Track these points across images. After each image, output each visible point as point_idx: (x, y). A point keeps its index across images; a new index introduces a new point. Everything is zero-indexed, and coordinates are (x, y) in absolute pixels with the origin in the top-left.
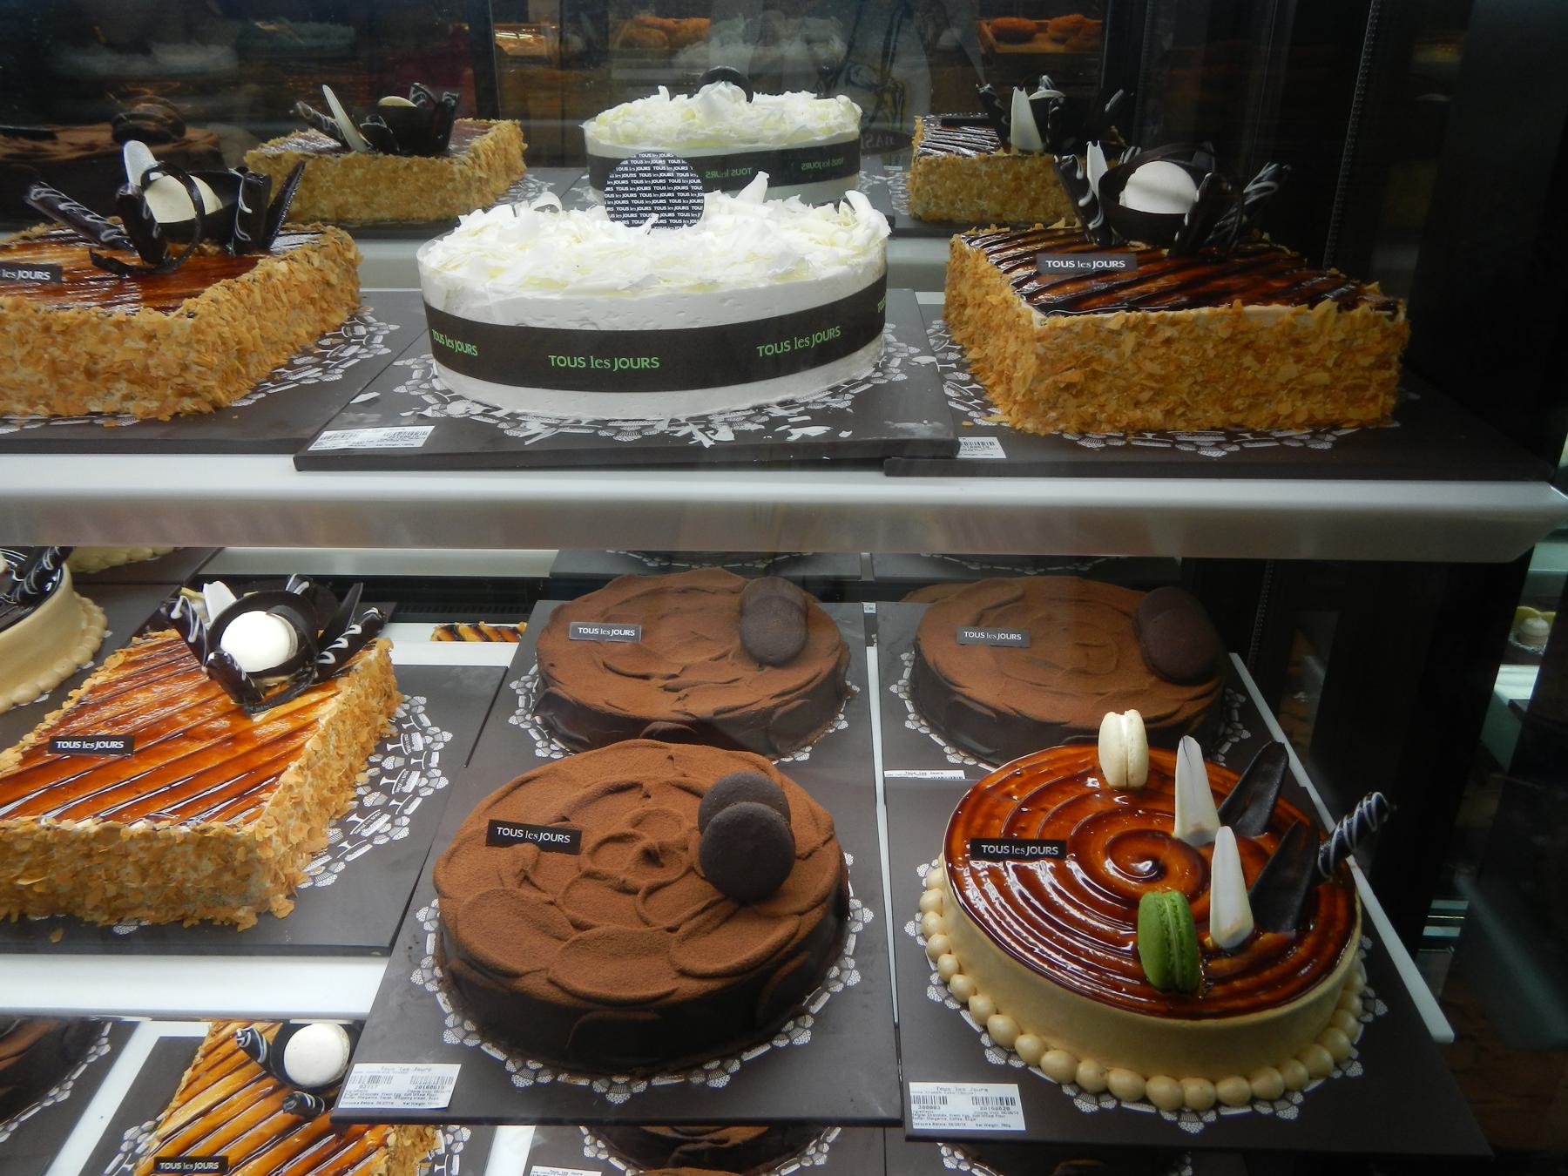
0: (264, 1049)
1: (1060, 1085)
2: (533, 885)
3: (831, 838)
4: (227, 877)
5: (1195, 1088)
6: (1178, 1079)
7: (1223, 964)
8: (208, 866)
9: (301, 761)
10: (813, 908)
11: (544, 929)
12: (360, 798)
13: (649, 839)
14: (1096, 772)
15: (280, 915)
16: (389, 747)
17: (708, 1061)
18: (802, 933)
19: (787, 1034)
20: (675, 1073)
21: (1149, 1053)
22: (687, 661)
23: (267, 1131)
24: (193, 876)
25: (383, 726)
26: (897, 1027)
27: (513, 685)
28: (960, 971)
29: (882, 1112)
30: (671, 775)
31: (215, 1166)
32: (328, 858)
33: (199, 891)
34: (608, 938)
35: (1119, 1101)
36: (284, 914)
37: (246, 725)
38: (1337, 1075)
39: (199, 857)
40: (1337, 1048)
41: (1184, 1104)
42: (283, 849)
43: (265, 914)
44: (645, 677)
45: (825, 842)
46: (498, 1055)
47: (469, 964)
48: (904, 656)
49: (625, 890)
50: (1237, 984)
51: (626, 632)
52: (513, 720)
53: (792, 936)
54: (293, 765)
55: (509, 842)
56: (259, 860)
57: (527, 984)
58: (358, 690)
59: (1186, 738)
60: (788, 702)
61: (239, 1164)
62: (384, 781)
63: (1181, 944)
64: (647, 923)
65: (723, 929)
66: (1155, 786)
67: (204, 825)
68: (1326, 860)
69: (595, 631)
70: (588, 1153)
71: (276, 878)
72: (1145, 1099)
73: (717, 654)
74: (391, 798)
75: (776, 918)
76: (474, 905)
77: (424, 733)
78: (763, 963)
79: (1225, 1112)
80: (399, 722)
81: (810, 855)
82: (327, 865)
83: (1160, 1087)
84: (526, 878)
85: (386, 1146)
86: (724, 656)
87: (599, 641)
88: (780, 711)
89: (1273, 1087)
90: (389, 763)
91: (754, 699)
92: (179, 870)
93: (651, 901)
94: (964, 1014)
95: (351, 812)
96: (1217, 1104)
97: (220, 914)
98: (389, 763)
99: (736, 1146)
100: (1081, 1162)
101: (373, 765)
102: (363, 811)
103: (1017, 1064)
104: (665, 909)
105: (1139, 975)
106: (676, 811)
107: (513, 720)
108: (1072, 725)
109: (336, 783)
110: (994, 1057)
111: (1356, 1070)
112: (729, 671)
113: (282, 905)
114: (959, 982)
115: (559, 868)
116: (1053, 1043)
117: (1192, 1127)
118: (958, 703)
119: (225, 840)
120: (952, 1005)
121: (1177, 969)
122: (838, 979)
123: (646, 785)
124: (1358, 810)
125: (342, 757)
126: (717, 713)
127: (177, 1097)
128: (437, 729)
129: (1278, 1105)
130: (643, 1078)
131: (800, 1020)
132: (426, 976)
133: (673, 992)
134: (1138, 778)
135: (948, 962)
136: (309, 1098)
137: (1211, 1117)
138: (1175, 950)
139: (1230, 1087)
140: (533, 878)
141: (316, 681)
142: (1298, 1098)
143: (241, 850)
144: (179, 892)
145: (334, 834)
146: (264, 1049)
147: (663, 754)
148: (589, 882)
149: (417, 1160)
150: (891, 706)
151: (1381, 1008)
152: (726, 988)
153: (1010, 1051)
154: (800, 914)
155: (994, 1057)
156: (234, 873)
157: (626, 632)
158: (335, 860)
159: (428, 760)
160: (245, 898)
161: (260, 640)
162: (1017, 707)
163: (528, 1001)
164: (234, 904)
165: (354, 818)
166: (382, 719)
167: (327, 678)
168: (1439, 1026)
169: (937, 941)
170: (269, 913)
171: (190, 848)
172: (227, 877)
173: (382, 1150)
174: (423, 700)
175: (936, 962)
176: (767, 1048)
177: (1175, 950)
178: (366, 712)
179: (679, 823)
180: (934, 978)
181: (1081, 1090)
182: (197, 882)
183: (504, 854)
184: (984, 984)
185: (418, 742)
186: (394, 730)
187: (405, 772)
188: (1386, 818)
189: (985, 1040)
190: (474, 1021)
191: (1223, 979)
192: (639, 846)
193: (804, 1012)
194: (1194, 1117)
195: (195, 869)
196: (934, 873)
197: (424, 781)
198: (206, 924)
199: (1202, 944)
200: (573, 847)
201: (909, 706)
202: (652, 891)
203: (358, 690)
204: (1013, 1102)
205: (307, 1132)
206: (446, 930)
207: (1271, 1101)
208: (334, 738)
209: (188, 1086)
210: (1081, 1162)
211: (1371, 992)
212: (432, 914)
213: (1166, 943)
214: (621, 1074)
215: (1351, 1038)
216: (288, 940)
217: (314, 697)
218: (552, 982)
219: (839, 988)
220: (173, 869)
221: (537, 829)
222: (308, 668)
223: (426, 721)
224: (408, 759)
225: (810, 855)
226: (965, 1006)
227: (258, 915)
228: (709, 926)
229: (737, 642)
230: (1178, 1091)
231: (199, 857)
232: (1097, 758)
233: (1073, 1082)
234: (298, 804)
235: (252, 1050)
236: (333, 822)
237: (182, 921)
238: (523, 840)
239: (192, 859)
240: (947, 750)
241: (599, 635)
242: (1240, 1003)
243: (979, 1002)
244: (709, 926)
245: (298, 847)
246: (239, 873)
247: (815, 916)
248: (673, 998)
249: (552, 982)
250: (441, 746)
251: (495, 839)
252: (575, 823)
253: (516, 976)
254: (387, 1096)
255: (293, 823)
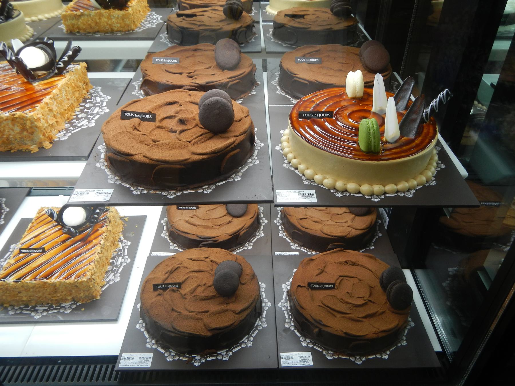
0: (55, 215)
1: (330, 190)
2: (138, 130)
3: (248, 115)
4: (25, 133)
5: (377, 188)
6: (372, 185)
7: (389, 146)
8: (17, 129)
9: (51, 96)
10: (241, 135)
11: (142, 142)
12: (77, 115)
13: (180, 116)
14: (345, 94)
15: (46, 148)
16: (88, 101)
17: (204, 186)
18: (237, 142)
19: (233, 178)
20: (192, 189)
21: (363, 175)
22: (195, 69)
23: (59, 241)
24: (12, 133)
25: (85, 94)
26: (272, 177)
27: (134, 83)
28: (295, 158)
29: (266, 198)
30: (190, 99)
31: (41, 251)
32: (65, 132)
33: (15, 139)
34: (166, 144)
35: (350, 193)
36: (49, 148)
37: (30, 86)
38: (427, 185)
39: (14, 125)
40: (428, 175)
41: (373, 194)
42: (46, 125)
43: (41, 148)
44: (180, 74)
45: (246, 117)
46: (128, 186)
47: (114, 153)
48: (276, 74)
49: (173, 131)
50: (394, 151)
51: (174, 61)
52: (133, 93)
53: (234, 143)
54: (48, 97)
55: (129, 118)
56: (36, 126)
57: (135, 158)
58: (73, 78)
59: (378, 74)
60: (233, 81)
61: (49, 250)
62: (86, 110)
63: (374, 134)
64: (180, 140)
65: (208, 142)
66: (365, 98)
67: (14, 113)
68: (426, 115)
69: (162, 60)
70: (171, 247)
71: (44, 135)
72: (359, 193)
73: (208, 66)
74: (88, 115)
75: (228, 138)
76: (115, 136)
77: (100, 97)
78: (222, 150)
79: (387, 195)
80: (91, 94)
81: (240, 120)
82: (64, 134)
83: (365, 188)
84: (135, 128)
85: (100, 244)
86: (210, 68)
87: (164, 64)
88: (230, 84)
89: (406, 186)
90: (87, 105)
91: (221, 79)
92: (7, 131)
93: (182, 134)
94: (296, 171)
95: (73, 119)
96: (385, 193)
97: (24, 148)
98: (87, 105)
99: (221, 242)
100: (336, 244)
101: (81, 106)
102: (78, 119)
103: (315, 184)
104: (185, 137)
105: (360, 150)
106: (191, 109)
107: (133, 93)
108: (336, 85)
109: (66, 108)
110: (306, 183)
111: (434, 183)
112: (211, 72)
113: (47, 145)
114: (294, 161)
115: (147, 126)
116: (327, 176)
117: (376, 200)
118: (296, 80)
119: (22, 118)
120: (292, 169)
121: (373, 144)
122: (251, 162)
123: (180, 102)
124: (439, 96)
125: (68, 99)
126: (207, 83)
127: (26, 231)
128: (105, 96)
129: (406, 193)
130: (180, 191)
131: (237, 174)
132: (102, 164)
133: (189, 159)
134: (360, 94)
135: (290, 156)
136: (72, 229)
137: (383, 197)
138: (372, 136)
139: (390, 187)
140: (138, 128)
141: (56, 74)
142: (413, 191)
143: (28, 121)
144: (8, 139)
145: (67, 125)
146: (55, 215)
147: (188, 94)
148: (157, 130)
149: (112, 251)
150: (271, 89)
151: (443, 166)
152: (208, 158)
153: (313, 181)
154: (236, 136)
155: (306, 183)
156: (27, 132)
157: (174, 61)
158: (67, 133)
159: (102, 104)
160: (33, 142)
161: (34, 58)
162: (316, 79)
163: (134, 163)
164: (29, 144)
165: (75, 121)
166: (84, 92)
167: (60, 72)
168: (463, 172)
169: (287, 150)
170: (43, 148)
171: (10, 122)
172: (25, 133)
173: (99, 245)
174: (100, 88)
175: (286, 157)
176: (225, 182)
177: (372, 136)
178: (77, 87)
179: (192, 113)
180: (286, 162)
181: (337, 191)
182: (14, 135)
183: (127, 122)
184: (305, 160)
185: (98, 99)
186: (90, 96)
187: (93, 108)
188: (449, 98)
189: (303, 178)
190: (118, 176)
191: (389, 150)
192: (177, 119)
193: (238, 172)
194: (377, 197)
195: (13, 130)
196: (286, 132)
197: (101, 110)
198: (20, 151)
199: (382, 141)
200: (153, 120)
201: (278, 87)
202: (182, 131)
203: (73, 78)
204: (313, 194)
205: (72, 241)
206: (109, 148)
207: (404, 192)
208: (64, 92)
209: (30, 229)
210: (336, 244)
211: (440, 162)
212: (103, 147)
213: (369, 133)
214: (172, 190)
215: (433, 174)
216: (50, 155)
217: (56, 79)
218: (144, 156)
219: (252, 165)
220: (4, 130)
221: (140, 113)
222: (54, 68)
223: (101, 93)
224: (94, 104)
225: (240, 120)
226: (297, 169)
227: (39, 148)
228: (203, 140)
229: (215, 63)
230: (371, 189)
231: (14, 125)
232: (345, 90)
233: (335, 189)
234: (51, 110)
235: (51, 215)
236: (67, 122)
237: (10, 150)
238: (134, 117)
239: (11, 126)
240: (291, 99)
241: (164, 62)
242: (395, 156)
243: (301, 167)
244: (203, 140)
245: (52, 126)
246: (29, 131)
247: (242, 137)
248: (189, 160)
249: (144, 156)
250: (107, 100)
251: (124, 116)
252: (153, 112)
253: (132, 155)
254: (133, 363)
255: (49, 117)
